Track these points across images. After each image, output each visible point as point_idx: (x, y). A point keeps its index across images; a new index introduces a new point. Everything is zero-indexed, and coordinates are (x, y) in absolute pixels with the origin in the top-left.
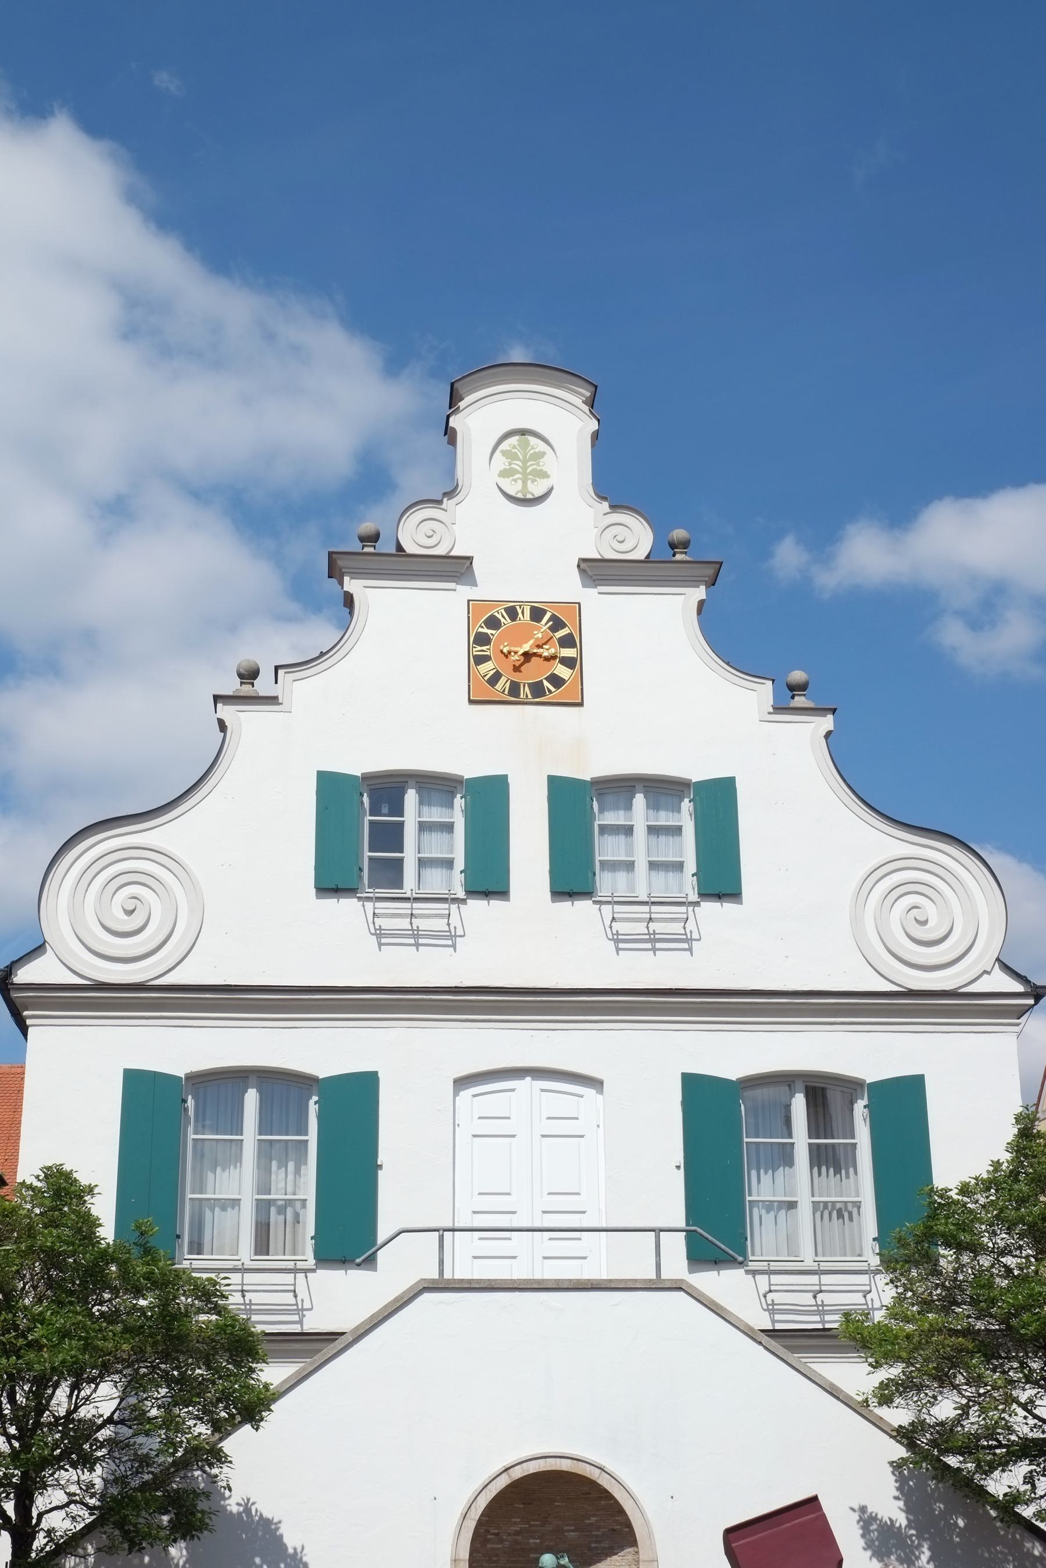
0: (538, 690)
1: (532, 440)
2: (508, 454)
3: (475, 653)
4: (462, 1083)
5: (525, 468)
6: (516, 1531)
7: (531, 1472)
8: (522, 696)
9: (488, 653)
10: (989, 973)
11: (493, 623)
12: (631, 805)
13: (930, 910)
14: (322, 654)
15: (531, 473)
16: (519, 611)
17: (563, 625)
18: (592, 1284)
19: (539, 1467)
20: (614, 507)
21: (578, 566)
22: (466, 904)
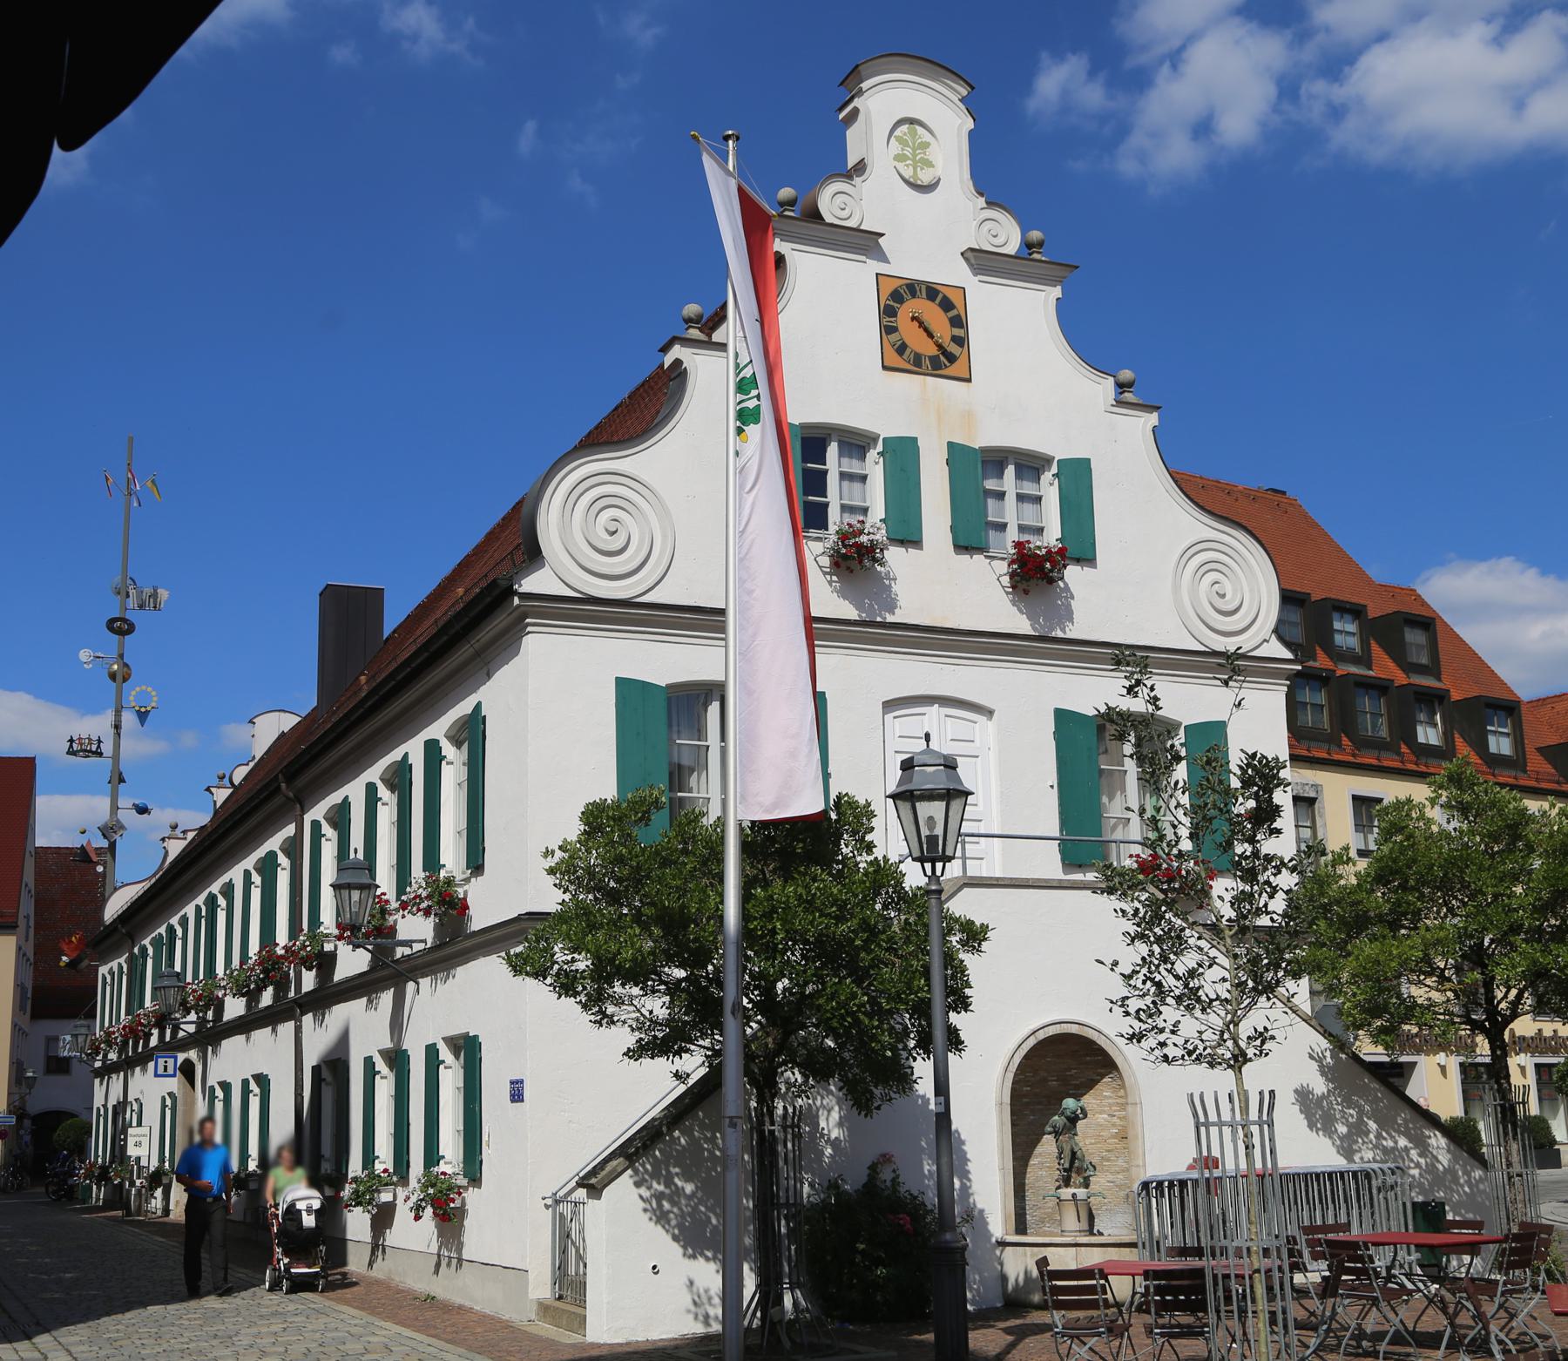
1: (920, 129)
2: (900, 140)
4: (890, 705)
5: (915, 155)
10: (1268, 641)
12: (1003, 473)
13: (1227, 587)
16: (918, 289)
20: (990, 204)
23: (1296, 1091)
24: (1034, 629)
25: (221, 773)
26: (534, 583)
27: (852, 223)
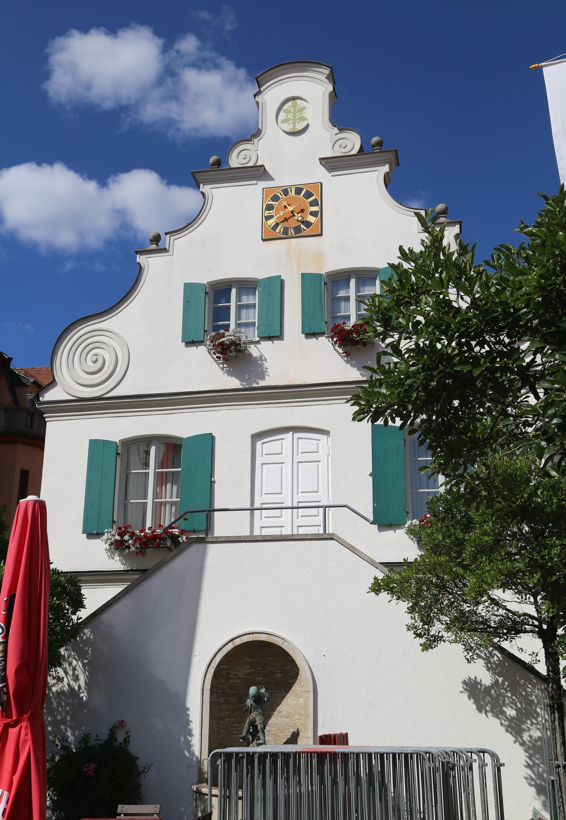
0: (298, 230)
1: (299, 102)
3: (266, 215)
5: (294, 117)
6: (248, 673)
7: (245, 641)
8: (289, 234)
9: (272, 214)
11: (275, 198)
14: (189, 225)
15: (297, 119)
16: (289, 191)
17: (312, 195)
18: (282, 537)
19: (250, 639)
20: (341, 130)
21: (321, 163)
22: (260, 344)
23: (464, 682)
24: (241, 385)
25: (186, 521)
26: (49, 396)
27: (251, 164)
